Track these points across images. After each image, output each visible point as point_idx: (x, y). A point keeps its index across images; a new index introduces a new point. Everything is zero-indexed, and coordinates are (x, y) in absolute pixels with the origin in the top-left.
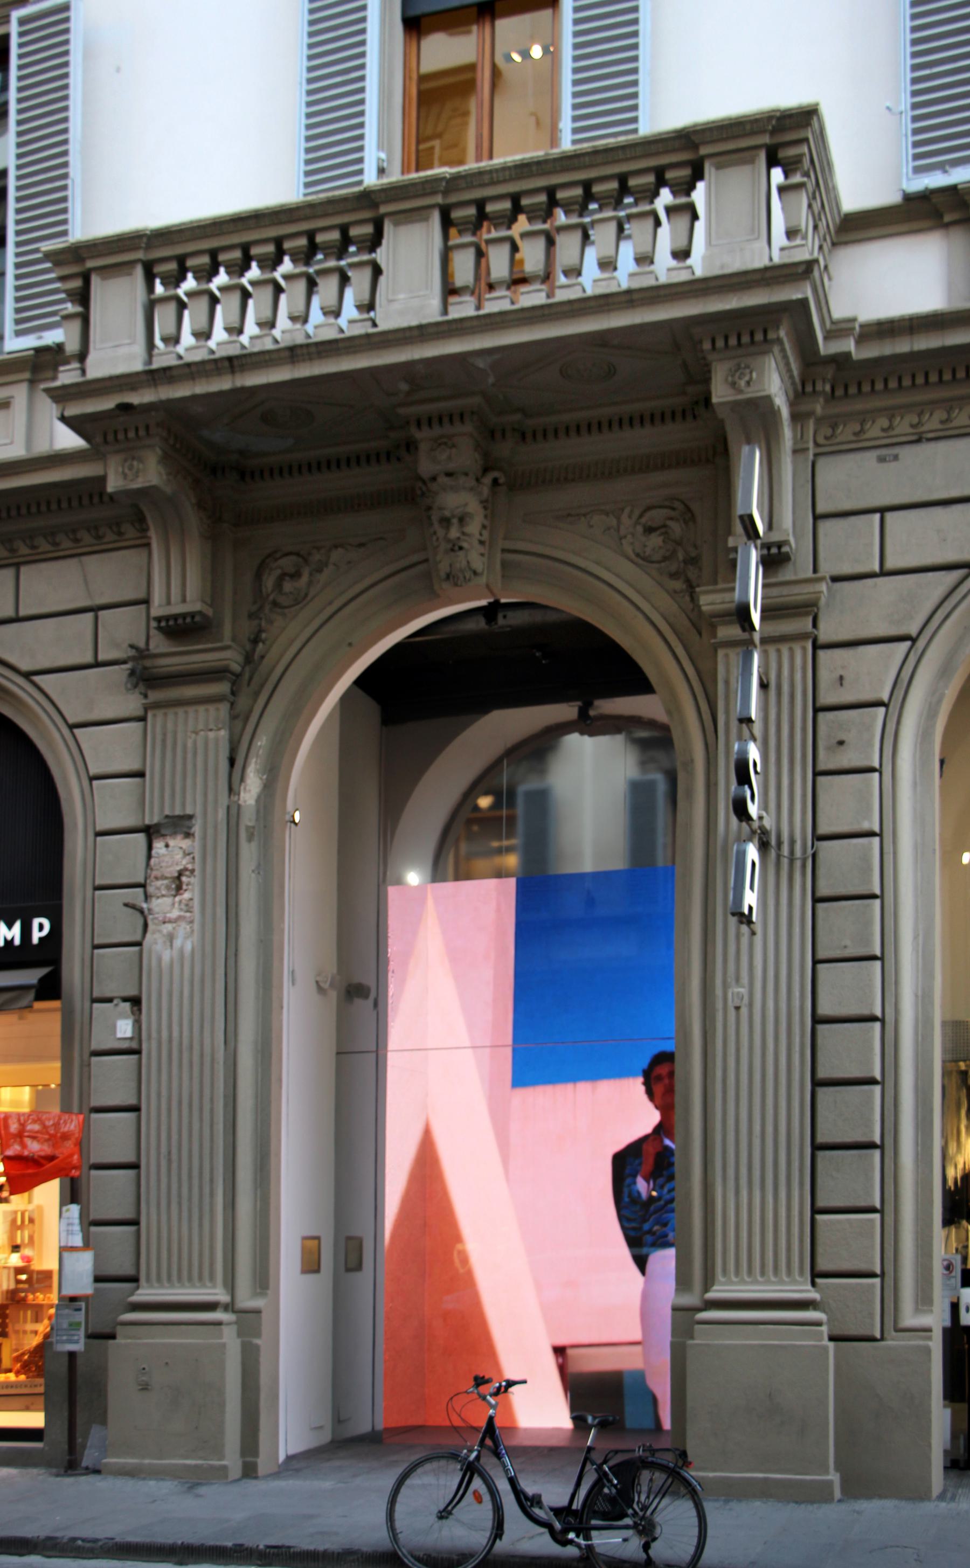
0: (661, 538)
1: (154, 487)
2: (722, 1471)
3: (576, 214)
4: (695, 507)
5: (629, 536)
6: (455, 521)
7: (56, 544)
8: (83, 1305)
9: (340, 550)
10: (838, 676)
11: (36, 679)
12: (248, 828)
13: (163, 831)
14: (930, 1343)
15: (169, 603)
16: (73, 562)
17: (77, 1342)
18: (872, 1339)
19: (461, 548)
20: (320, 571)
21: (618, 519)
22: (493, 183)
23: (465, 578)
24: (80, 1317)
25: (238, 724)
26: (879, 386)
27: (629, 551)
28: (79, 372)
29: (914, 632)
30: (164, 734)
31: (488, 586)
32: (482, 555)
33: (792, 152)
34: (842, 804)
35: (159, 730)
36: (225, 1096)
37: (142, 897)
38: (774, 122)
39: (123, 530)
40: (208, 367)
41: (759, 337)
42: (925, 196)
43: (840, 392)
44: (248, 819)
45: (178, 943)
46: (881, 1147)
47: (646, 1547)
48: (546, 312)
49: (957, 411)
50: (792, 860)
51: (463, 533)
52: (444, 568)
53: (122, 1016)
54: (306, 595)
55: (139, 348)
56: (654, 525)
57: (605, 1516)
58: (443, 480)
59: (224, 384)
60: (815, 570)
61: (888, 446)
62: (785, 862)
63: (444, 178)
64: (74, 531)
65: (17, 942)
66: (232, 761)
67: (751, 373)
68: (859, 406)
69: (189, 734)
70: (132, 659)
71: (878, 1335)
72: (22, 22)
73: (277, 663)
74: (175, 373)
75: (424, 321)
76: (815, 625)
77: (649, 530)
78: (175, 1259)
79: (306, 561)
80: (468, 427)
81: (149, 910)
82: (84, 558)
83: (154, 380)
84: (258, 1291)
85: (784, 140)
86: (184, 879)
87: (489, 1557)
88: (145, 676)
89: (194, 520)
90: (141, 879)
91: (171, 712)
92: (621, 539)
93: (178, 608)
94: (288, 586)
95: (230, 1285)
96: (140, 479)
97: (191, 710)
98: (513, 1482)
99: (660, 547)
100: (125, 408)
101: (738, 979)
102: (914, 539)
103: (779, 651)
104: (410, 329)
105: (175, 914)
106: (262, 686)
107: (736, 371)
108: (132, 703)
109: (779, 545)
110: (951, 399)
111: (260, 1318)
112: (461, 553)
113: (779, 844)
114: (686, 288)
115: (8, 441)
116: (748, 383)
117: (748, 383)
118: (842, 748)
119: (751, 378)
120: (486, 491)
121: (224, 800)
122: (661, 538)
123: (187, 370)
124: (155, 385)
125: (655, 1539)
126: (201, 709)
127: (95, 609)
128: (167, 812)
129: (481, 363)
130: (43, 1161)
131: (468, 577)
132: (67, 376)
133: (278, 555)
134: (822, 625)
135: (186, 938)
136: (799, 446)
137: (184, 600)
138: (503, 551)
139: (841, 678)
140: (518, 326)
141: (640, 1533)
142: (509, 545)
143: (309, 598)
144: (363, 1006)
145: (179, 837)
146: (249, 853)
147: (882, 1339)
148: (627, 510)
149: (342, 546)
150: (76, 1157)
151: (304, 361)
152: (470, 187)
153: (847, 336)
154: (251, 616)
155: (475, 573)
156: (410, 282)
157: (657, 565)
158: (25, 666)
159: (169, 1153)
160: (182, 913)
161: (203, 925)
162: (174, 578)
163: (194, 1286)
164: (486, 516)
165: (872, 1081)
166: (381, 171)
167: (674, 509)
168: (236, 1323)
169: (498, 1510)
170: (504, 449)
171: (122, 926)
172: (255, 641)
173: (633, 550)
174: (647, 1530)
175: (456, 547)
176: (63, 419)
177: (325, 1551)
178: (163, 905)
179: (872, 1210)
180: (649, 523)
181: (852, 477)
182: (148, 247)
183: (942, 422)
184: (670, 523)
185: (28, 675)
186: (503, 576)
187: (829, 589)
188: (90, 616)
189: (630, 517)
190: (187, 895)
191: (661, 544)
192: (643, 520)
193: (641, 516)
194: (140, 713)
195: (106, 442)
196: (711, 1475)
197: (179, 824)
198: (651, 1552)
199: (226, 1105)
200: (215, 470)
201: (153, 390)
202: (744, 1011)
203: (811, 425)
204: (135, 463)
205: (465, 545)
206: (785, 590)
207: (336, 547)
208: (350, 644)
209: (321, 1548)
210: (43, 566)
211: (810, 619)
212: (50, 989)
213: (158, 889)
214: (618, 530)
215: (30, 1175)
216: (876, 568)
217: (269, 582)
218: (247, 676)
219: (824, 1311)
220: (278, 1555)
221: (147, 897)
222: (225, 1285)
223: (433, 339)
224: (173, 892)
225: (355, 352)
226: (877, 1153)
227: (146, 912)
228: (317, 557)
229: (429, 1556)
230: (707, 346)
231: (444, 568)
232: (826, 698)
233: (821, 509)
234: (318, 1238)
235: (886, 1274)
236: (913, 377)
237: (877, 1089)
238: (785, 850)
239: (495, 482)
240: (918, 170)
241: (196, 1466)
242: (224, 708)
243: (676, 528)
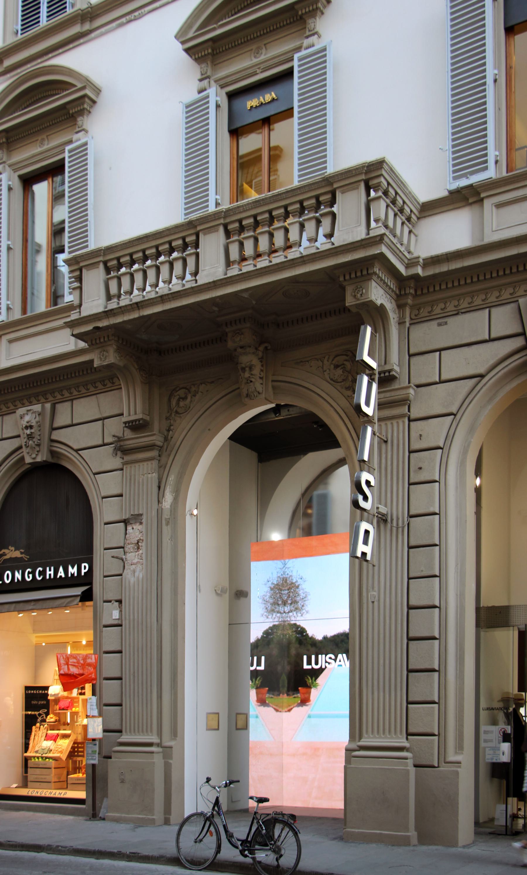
0: (342, 370)
2: (362, 829)
3: (282, 221)
6: (247, 369)
7: (88, 389)
8: (97, 743)
9: (203, 385)
10: (418, 435)
11: (80, 452)
12: (166, 519)
13: (131, 522)
14: (459, 769)
16: (94, 397)
17: (95, 759)
18: (434, 767)
19: (251, 381)
20: (195, 396)
21: (323, 362)
22: (244, 211)
24: (97, 748)
26: (437, 288)
27: (327, 377)
28: (194, 282)
29: (455, 412)
30: (131, 476)
31: (266, 399)
32: (262, 384)
33: (375, 181)
34: (423, 499)
36: (157, 646)
37: (123, 553)
38: (365, 168)
39: (114, 381)
40: (128, 308)
41: (365, 272)
43: (419, 292)
44: (166, 515)
45: (137, 574)
46: (438, 671)
47: (277, 860)
49: (504, 291)
50: (397, 528)
51: (252, 374)
52: (245, 392)
53: (115, 609)
54: (190, 407)
57: (260, 844)
58: (239, 350)
59: (135, 315)
60: (409, 383)
61: (442, 318)
62: (394, 529)
63: (223, 211)
64: (95, 383)
65: (76, 575)
66: (159, 487)
67: (362, 290)
68: (430, 298)
70: (116, 441)
71: (436, 765)
72: (70, 152)
73: (177, 440)
75: (215, 279)
76: (409, 411)
77: (336, 367)
78: (136, 722)
79: (190, 392)
81: (126, 559)
82: (98, 395)
83: (107, 315)
84: (173, 738)
85: (371, 177)
86: (140, 544)
87: (215, 861)
88: (122, 449)
90: (122, 545)
91: (133, 465)
92: (324, 372)
95: (160, 734)
96: (107, 360)
97: (137, 465)
98: (225, 827)
99: (342, 375)
100: (97, 328)
101: (373, 588)
102: (456, 363)
103: (392, 423)
104: (210, 283)
105: (136, 560)
107: (356, 290)
108: (117, 462)
109: (389, 371)
110: (473, 292)
111: (172, 750)
112: (251, 384)
113: (392, 520)
114: (327, 253)
115: (68, 343)
118: (421, 471)
119: (363, 292)
120: (260, 354)
121: (155, 506)
122: (342, 370)
123: (120, 310)
124: (108, 318)
125: (281, 856)
126: (145, 463)
127: (103, 419)
128: (132, 513)
129: (246, 295)
130: (78, 676)
132: (74, 316)
133: (178, 389)
134: (412, 410)
135: (140, 572)
136: (401, 321)
137: (136, 414)
138: (273, 381)
139: (421, 435)
140: (241, 281)
141: (274, 851)
142: (275, 378)
144: (243, 600)
145: (138, 524)
146: (166, 531)
147: (438, 767)
148: (327, 357)
150: (93, 674)
151: (167, 301)
152: (235, 214)
153: (417, 265)
154: (167, 418)
155: (259, 393)
156: (212, 261)
157: (339, 384)
158: (75, 447)
159: (134, 673)
160: (139, 560)
161: (147, 565)
162: (126, 403)
163: (144, 735)
164: (262, 366)
165: (434, 638)
166: (217, 204)
167: (347, 355)
168: (162, 752)
169: (219, 839)
171: (114, 567)
172: (169, 430)
173: (329, 377)
174: (278, 852)
176: (73, 335)
177: (152, 856)
178: (132, 557)
179: (434, 702)
180: (337, 363)
181: (427, 335)
182: (104, 255)
183: (469, 304)
184: (345, 362)
185: (77, 451)
186: (274, 393)
187: (415, 391)
189: (328, 361)
190: (141, 552)
191: (342, 373)
192: (334, 362)
193: (333, 360)
196: (357, 830)
197: (137, 518)
198: (279, 861)
199: (157, 650)
202: (376, 603)
203: (408, 311)
204: (105, 353)
205: (253, 380)
206: (393, 394)
207: (201, 384)
208: (209, 430)
209: (151, 854)
210: (82, 400)
211: (407, 407)
212: (87, 596)
213: (129, 549)
214: (323, 368)
215: (71, 683)
216: (438, 380)
217: (174, 402)
218: (165, 447)
219: (411, 752)
220: (134, 857)
221: (125, 553)
222: (158, 735)
223: (220, 287)
224: (136, 550)
225: (188, 296)
226: (436, 674)
227: (124, 560)
229: (192, 859)
230: (342, 279)
231: (245, 392)
232: (414, 447)
233: (411, 352)
234: (218, 714)
235: (440, 735)
236: (459, 280)
237: (436, 642)
238: (395, 524)
239: (266, 348)
240: (455, 178)
241: (142, 818)
242: (155, 463)
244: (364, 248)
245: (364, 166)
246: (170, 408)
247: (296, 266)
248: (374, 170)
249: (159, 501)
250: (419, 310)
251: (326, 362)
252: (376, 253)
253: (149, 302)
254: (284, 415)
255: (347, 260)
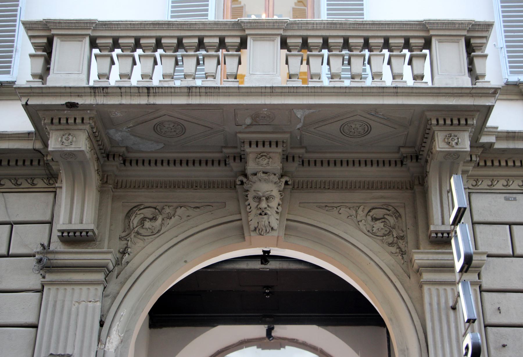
1: (82, 151)
4: (401, 211)
5: (363, 221)
15: (70, 222)
23: (266, 231)
25: (108, 300)
30: (55, 302)
35: (51, 298)
42: (517, 84)
48: (347, 91)
51: (268, 206)
52: (253, 224)
55: (84, 76)
56: (378, 217)
58: (260, 175)
59: (143, 101)
61: (509, 193)
66: (102, 324)
69: (74, 303)
74: (109, 90)
75: (274, 85)
76: (479, 279)
77: (375, 219)
80: (280, 150)
88: (47, 265)
89: (94, 179)
91: (62, 288)
93: (76, 226)
94: (148, 224)
96: (73, 146)
97: (77, 288)
100: (72, 106)
106: (127, 279)
112: (265, 217)
116: (457, 144)
117: (457, 144)
119: (458, 141)
122: (383, 223)
127: (12, 224)
128: (52, 351)
131: (268, 231)
133: (142, 207)
138: (287, 220)
139: (499, 309)
142: (291, 217)
143: (161, 232)
148: (362, 207)
149: (184, 206)
155: (272, 229)
167: (389, 210)
170: (293, 167)
172: (124, 253)
175: (262, 213)
180: (374, 216)
188: (8, 226)
192: (371, 214)
193: (369, 211)
194: (39, 287)
195: (52, 123)
200: (108, 156)
201: (93, 98)
204: (70, 137)
205: (268, 212)
208: (186, 262)
217: (135, 221)
228: (167, 210)
230: (434, 122)
231: (253, 224)
239: (286, 183)
242: (100, 288)
243: (392, 220)
244: (473, 96)
245: (471, 23)
246: (127, 227)
247: (386, 95)
248: (478, 31)
249: (99, 340)
250: (477, 181)
251: (360, 211)
252: (487, 104)
253: (169, 90)
254: (273, 265)
255: (451, 103)
